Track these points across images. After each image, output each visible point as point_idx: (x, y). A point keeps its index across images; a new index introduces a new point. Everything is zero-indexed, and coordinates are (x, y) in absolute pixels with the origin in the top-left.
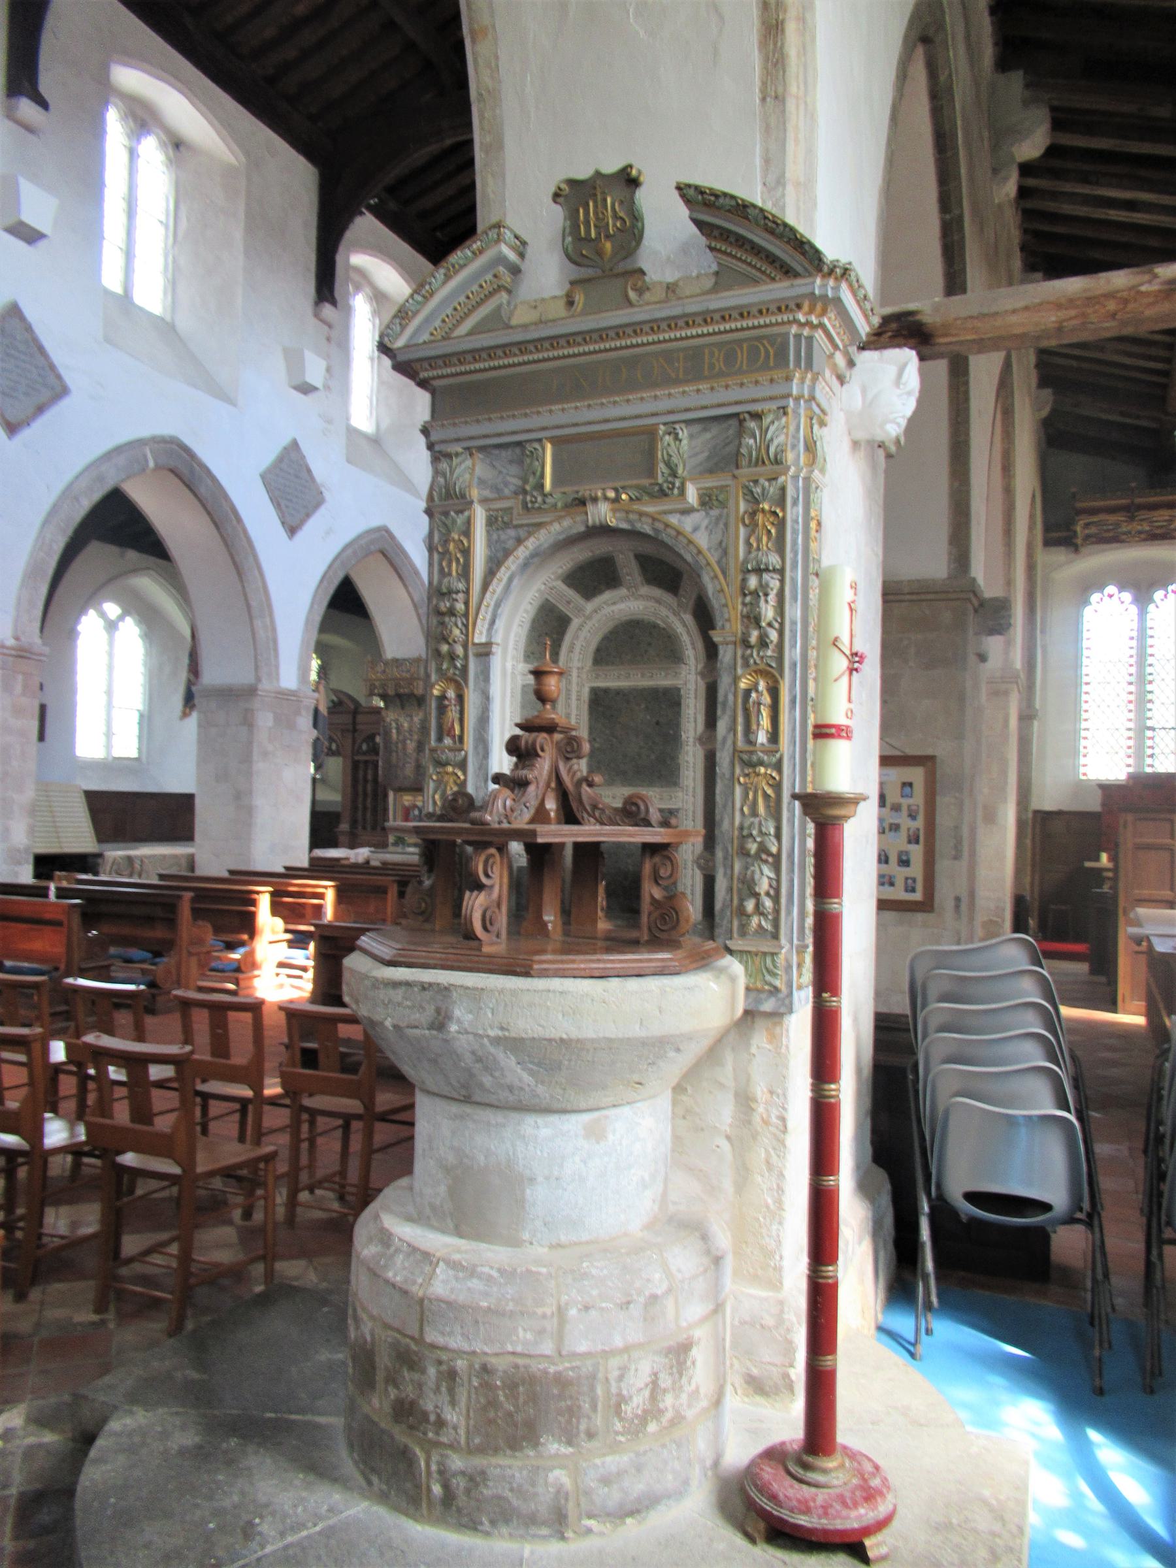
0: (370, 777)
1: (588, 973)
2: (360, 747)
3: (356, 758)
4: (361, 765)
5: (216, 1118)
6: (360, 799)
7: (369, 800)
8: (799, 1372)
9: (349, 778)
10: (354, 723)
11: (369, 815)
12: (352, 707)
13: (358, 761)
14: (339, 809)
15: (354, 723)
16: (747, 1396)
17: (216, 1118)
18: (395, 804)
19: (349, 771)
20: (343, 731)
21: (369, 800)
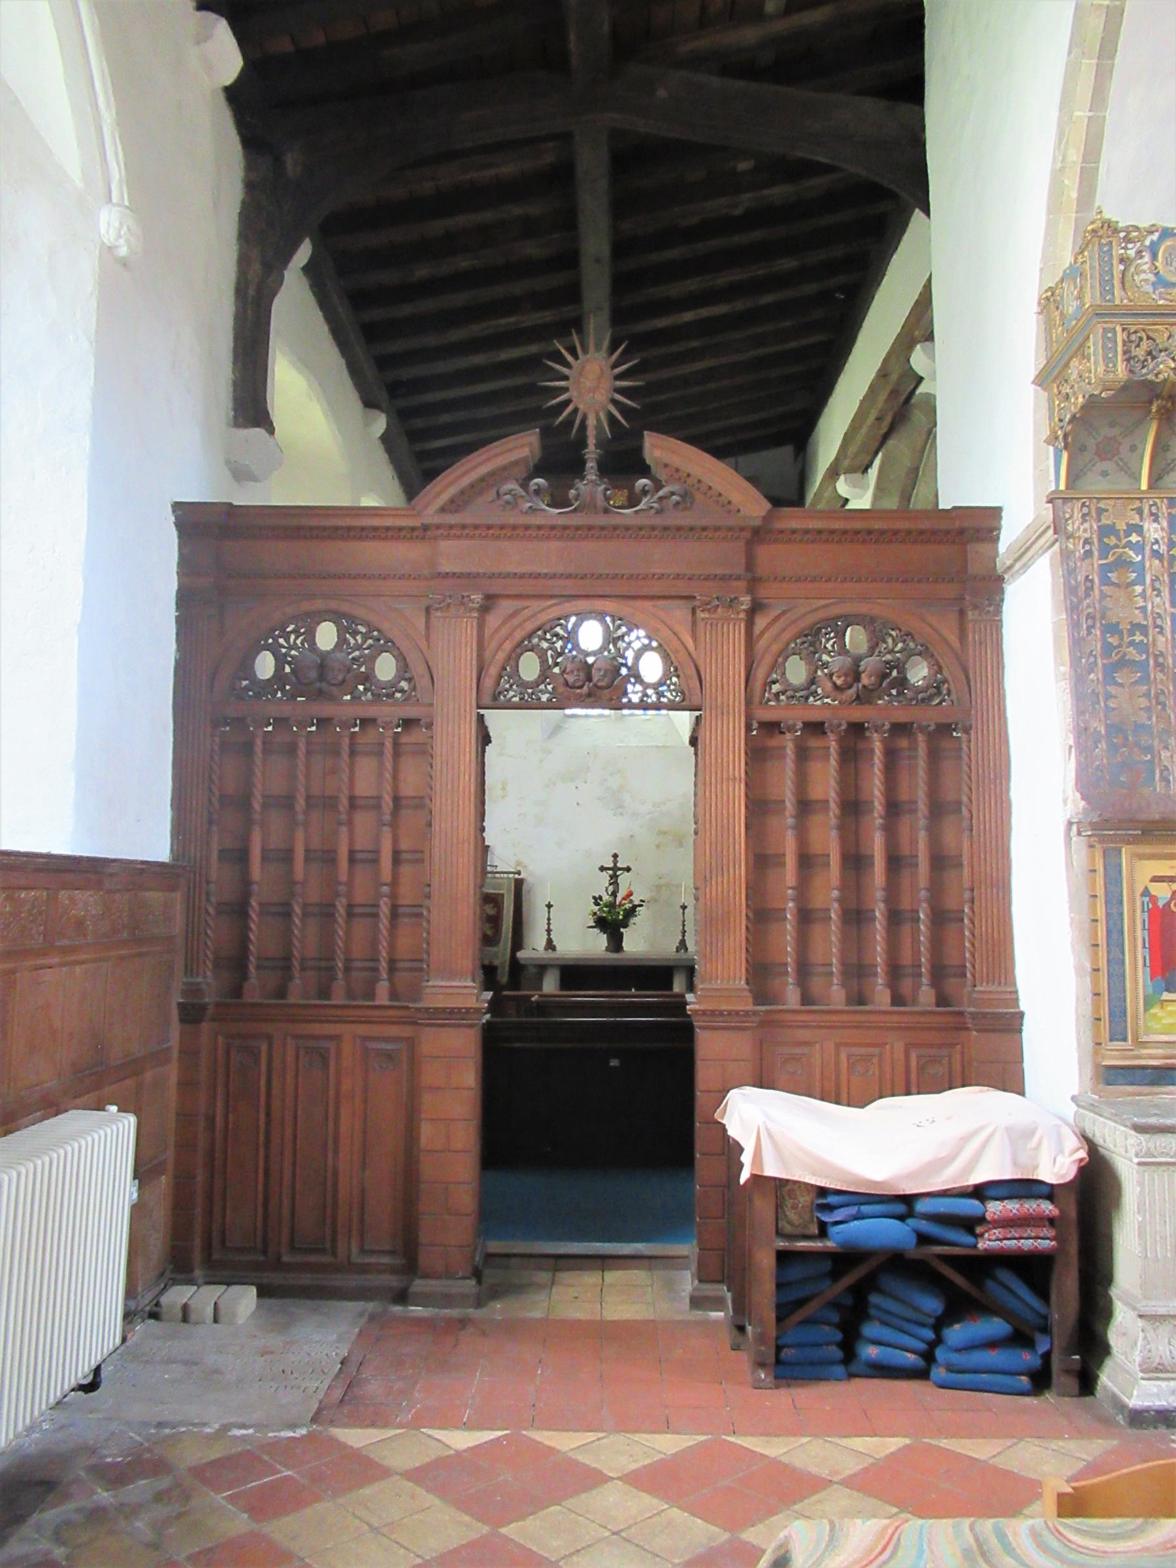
5: (738, 578)
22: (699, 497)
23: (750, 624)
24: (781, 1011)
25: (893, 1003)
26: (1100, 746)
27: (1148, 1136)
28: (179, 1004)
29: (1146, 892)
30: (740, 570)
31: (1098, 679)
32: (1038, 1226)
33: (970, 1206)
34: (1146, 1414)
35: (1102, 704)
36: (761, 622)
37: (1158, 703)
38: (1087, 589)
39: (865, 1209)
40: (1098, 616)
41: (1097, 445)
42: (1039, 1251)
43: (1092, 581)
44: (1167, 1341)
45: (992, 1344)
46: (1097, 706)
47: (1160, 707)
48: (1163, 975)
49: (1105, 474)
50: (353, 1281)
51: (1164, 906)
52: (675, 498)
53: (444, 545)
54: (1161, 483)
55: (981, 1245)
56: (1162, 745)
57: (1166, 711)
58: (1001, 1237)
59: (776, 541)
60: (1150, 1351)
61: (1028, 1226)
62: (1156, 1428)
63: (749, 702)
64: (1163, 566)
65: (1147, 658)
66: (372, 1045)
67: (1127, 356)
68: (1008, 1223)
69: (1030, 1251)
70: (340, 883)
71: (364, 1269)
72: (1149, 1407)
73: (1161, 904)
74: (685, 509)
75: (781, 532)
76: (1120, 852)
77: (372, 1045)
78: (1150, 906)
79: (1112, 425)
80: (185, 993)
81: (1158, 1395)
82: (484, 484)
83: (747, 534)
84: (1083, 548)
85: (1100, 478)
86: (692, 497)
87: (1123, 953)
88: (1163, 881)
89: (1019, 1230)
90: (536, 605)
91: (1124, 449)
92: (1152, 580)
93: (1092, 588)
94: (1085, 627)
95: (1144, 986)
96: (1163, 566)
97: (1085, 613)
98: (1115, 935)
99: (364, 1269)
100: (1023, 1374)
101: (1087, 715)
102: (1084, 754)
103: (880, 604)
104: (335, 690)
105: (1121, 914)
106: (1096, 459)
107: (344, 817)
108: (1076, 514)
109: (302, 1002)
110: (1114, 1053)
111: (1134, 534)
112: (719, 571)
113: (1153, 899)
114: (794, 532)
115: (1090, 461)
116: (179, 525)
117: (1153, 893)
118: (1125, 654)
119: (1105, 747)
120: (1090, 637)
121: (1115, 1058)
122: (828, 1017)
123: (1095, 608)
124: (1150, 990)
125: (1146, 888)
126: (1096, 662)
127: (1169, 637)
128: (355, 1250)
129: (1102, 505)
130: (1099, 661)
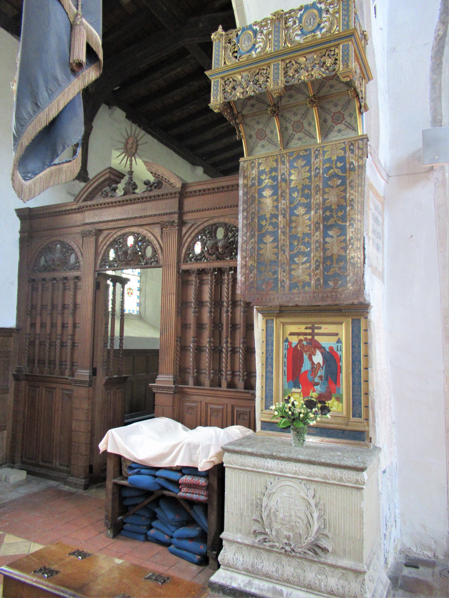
0: (207, 297)
1: (284, 383)
2: (191, 248)
3: (184, 267)
4: (193, 278)
5: (175, 213)
6: (191, 333)
7: (206, 334)
8: (291, 456)
9: (173, 299)
10: (181, 212)
11: (206, 357)
12: (179, 185)
13: (187, 272)
14: (157, 347)
15: (181, 212)
16: (55, 154)
17: (175, 213)
18: (268, 343)
19: (173, 288)
20: (163, 226)
21: (206, 334)
22: (164, 182)
23: (180, 231)
24: (187, 388)
25: (245, 388)
26: (253, 272)
27: (230, 454)
28: (14, 375)
29: (287, 340)
30: (176, 210)
31: (255, 241)
32: (200, 489)
33: (174, 476)
34: (214, 585)
35: (256, 253)
36: (184, 230)
37: (282, 250)
38: (252, 200)
39: (143, 471)
40: (256, 212)
41: (256, 133)
42: (199, 501)
43: (255, 197)
44: (233, 553)
45: (191, 539)
46: (253, 254)
47: (282, 252)
48: (293, 380)
49: (263, 146)
50: (56, 474)
51: (295, 347)
52: (155, 185)
53: (87, 213)
54: (289, 146)
55: (179, 494)
56: (282, 270)
57: (285, 254)
58: (185, 491)
59: (190, 196)
60: (224, 556)
61: (197, 488)
62: (219, 593)
63: (179, 262)
64: (286, 185)
65: (278, 230)
66: (64, 392)
67: (224, 91)
68: (190, 486)
69: (196, 500)
70: (57, 335)
71: (60, 471)
72: (217, 582)
73: (293, 345)
74: (159, 188)
75: (191, 192)
76: (273, 320)
77: (64, 392)
78: (288, 347)
79: (258, 123)
80: (17, 371)
81: (224, 578)
82: (98, 190)
83: (178, 195)
84: (251, 182)
85: (261, 149)
86: (162, 183)
87: (272, 368)
88: (295, 335)
89: (193, 489)
90: (114, 231)
91: (268, 132)
92: (281, 193)
93: (254, 200)
94: (250, 218)
95: (283, 386)
96: (286, 185)
97: (251, 212)
98: (269, 360)
99: (60, 471)
100: (198, 555)
101: (247, 259)
102: (244, 276)
103: (229, 217)
104: (57, 268)
105: (273, 350)
106: (258, 140)
107: (60, 312)
108: (249, 167)
109: (49, 375)
110: (266, 415)
111: (274, 172)
112: (168, 211)
113: (290, 343)
114: (195, 192)
115: (256, 142)
116: (18, 215)
117: (290, 340)
118: (268, 229)
119: (256, 273)
120: (252, 223)
121: (267, 418)
122: (202, 391)
123: (255, 209)
124: (286, 387)
125: (287, 338)
126: (254, 235)
127: (288, 218)
128: (58, 463)
129: (260, 161)
130: (256, 233)
